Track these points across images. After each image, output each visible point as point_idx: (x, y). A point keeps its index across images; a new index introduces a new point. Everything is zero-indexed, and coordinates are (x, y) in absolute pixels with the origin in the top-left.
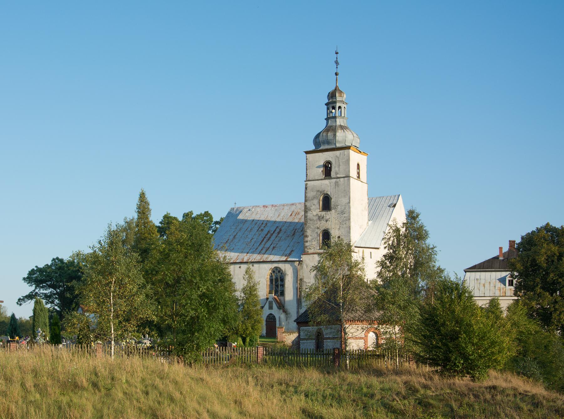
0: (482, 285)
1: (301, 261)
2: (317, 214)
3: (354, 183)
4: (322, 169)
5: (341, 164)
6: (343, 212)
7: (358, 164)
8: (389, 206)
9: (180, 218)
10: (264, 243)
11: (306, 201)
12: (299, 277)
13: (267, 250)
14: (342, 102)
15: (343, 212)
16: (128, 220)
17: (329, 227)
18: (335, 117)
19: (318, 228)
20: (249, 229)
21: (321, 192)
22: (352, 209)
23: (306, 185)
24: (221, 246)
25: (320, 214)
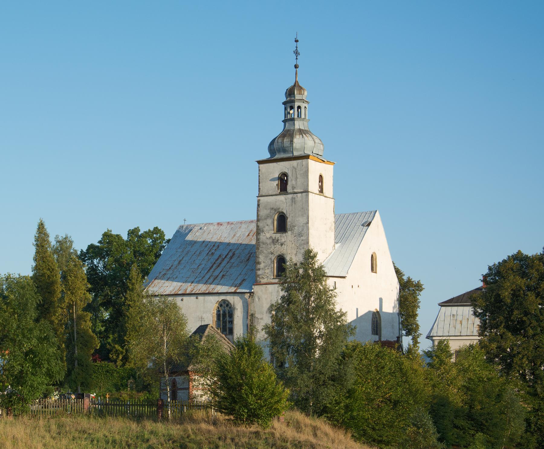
0: (458, 322)
1: (253, 293)
2: (271, 237)
3: (314, 200)
4: (277, 182)
5: (298, 176)
6: (300, 235)
7: (321, 177)
8: (363, 225)
9: (125, 237)
10: (212, 270)
11: (258, 220)
12: (250, 312)
13: (214, 279)
14: (302, 100)
15: (300, 235)
16: (60, 239)
17: (284, 252)
18: (293, 120)
19: (272, 253)
20: (198, 253)
21: (275, 210)
22: (310, 231)
23: (259, 201)
24: (163, 273)
25: (274, 236)
